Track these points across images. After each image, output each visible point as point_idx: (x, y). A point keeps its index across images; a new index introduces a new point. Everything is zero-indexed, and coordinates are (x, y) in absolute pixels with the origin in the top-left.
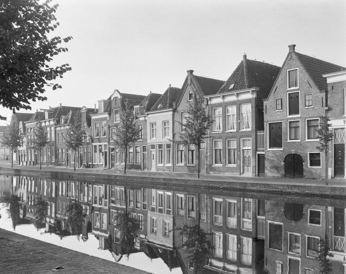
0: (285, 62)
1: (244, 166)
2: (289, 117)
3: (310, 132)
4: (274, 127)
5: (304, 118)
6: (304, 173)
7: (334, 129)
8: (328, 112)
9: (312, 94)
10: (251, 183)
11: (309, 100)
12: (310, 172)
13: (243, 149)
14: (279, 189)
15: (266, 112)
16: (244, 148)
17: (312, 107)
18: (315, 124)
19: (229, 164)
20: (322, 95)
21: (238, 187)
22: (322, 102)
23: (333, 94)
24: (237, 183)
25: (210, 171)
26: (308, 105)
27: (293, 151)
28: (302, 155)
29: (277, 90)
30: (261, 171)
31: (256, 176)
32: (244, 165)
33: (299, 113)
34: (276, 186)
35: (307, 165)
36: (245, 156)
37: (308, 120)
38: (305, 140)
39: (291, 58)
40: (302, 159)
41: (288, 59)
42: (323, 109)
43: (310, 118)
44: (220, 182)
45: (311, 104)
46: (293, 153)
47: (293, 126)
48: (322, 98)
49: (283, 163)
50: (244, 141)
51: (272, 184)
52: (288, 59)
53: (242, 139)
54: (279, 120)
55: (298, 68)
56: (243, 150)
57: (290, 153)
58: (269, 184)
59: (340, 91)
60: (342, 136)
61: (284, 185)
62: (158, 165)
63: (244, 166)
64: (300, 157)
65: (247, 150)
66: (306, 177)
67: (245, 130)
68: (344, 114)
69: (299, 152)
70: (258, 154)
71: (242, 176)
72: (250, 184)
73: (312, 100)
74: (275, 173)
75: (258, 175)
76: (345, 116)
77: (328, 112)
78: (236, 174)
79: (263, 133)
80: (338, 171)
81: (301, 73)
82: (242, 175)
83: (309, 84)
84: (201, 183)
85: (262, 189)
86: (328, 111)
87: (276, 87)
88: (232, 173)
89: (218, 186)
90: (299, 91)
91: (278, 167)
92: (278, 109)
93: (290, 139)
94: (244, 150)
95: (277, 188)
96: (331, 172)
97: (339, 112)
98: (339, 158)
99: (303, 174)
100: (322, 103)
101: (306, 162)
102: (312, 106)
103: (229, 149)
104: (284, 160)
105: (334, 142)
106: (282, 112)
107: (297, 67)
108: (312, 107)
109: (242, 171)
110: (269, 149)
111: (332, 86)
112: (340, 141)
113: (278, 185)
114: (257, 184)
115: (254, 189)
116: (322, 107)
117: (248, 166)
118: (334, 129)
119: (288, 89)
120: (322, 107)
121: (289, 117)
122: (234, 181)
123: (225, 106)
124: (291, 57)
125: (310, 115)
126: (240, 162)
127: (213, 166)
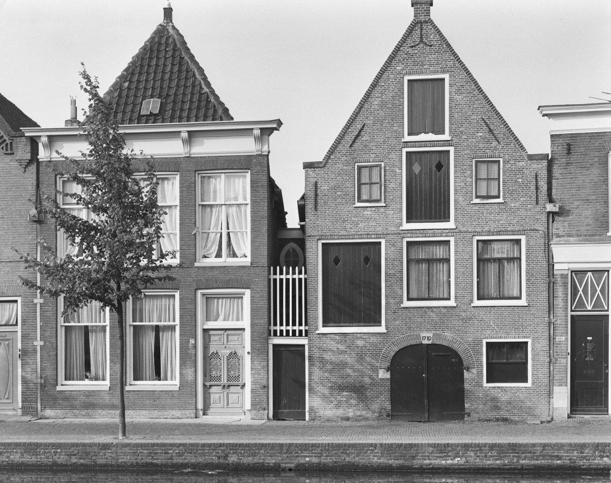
0: (397, 49)
1: (211, 386)
2: (407, 226)
3: (484, 274)
4: (341, 258)
5: (470, 235)
6: (467, 405)
7: (572, 272)
8: (553, 222)
9: (499, 161)
10: (434, 446)
11: (371, 184)
12: (495, 403)
13: (205, 327)
14: (560, 459)
15: (316, 209)
16: (210, 325)
17: (501, 200)
18: (514, 253)
19: (135, 379)
20: (535, 166)
21: (376, 460)
22: (537, 188)
23: (572, 168)
24: (371, 445)
25: (44, 408)
26: (484, 194)
27: (426, 337)
28: (455, 346)
29: (365, 137)
30: (284, 401)
31: (268, 419)
32: (208, 384)
33: (449, 217)
34: (549, 452)
35: (476, 377)
36: (212, 350)
37: (408, 242)
38: (472, 301)
39: (421, 41)
40: (460, 361)
41: (409, 41)
42: (538, 209)
43: (489, 233)
44: (281, 445)
45: (495, 193)
46: (425, 342)
47: (425, 260)
48: (536, 176)
49: (384, 374)
50: (208, 298)
51: (534, 445)
52: (410, 42)
53: (203, 295)
54: (368, 235)
55: (446, 76)
56: (205, 331)
57: (413, 342)
58: (520, 445)
59: (596, 160)
60: (581, 292)
61: (583, 446)
62: (127, 388)
63: (211, 386)
64: (455, 354)
65: (226, 330)
66: (475, 416)
67: (212, 261)
68: (607, 230)
69: (448, 338)
70: (274, 346)
71: (203, 420)
72: (431, 449)
73: (499, 179)
74: (351, 406)
75: (276, 417)
76: (609, 234)
77: (553, 222)
78: (184, 417)
79: (284, 277)
80: (587, 394)
81: (459, 92)
82: (204, 417)
83: (491, 130)
84: (180, 455)
85: (489, 462)
86: (553, 216)
87: (359, 127)
88: (156, 413)
89: (271, 461)
90: (452, 149)
91: (362, 386)
92: (364, 197)
93: (409, 299)
94: (211, 332)
95: (552, 456)
96: (562, 398)
97: (591, 222)
98: (586, 357)
99: (463, 408)
100: (537, 191)
101: (474, 371)
102: (498, 197)
103: (135, 327)
104: (388, 364)
105: (572, 311)
106: (382, 210)
107: (443, 72)
108: (501, 200)
109: (200, 406)
110: (322, 330)
111: (569, 145)
112: (589, 308)
113: (560, 446)
114: (466, 447)
115: (452, 465)
116: (537, 203)
117: (229, 386)
118: (572, 272)
119: (407, 138)
120: (537, 203)
121: (407, 226)
122: (18, 441)
123: (195, 171)
124: (421, 38)
125: (493, 227)
126: (196, 371)
127: (59, 388)
